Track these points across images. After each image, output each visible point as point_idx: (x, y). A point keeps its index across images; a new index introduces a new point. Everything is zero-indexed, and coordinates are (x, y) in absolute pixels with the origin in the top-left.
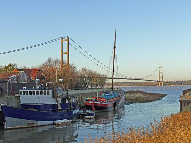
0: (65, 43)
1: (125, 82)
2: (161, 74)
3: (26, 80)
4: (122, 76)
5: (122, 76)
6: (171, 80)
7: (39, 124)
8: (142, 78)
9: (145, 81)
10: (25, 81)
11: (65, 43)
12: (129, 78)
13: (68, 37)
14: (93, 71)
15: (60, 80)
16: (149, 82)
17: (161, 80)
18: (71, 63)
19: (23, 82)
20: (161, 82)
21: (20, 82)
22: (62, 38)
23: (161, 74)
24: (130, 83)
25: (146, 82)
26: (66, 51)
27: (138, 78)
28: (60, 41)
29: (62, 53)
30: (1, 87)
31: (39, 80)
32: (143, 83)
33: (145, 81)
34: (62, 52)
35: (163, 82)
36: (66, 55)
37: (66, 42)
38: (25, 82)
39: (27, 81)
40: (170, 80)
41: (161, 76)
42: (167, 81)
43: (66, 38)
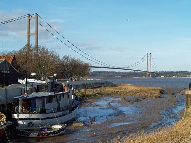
0: (33, 22)
2: (149, 63)
3: (8, 69)
4: (103, 64)
5: (103, 64)
6: (161, 70)
7: (40, 121)
9: (129, 71)
10: (6, 70)
11: (33, 22)
13: (37, 14)
14: (76, 59)
15: (55, 75)
17: (149, 71)
18: (39, 44)
19: (5, 72)
21: (2, 72)
22: (29, 15)
23: (149, 63)
24: (112, 72)
25: (130, 72)
27: (122, 67)
28: (27, 19)
29: (29, 34)
36: (35, 37)
38: (7, 72)
39: (9, 70)
40: (159, 70)
41: (149, 65)
42: (157, 71)
43: (35, 16)
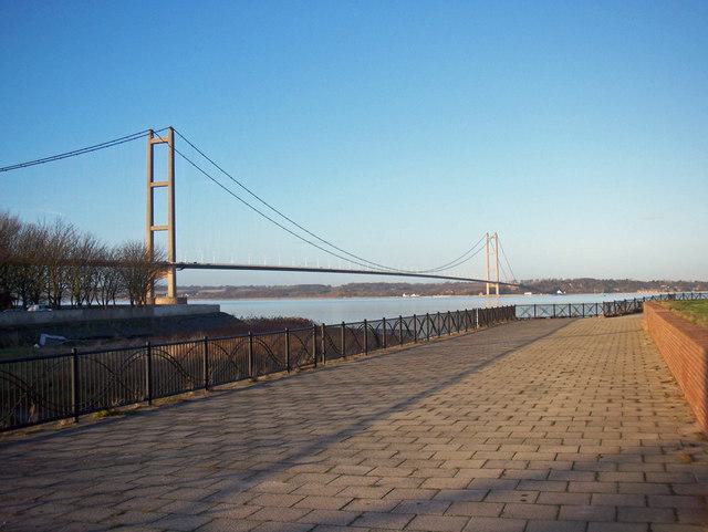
0: (162, 153)
1: (381, 284)
8: (432, 271)
9: (443, 281)
11: (162, 153)
12: (385, 270)
16: (456, 284)
20: (494, 283)
25: (447, 284)
26: (166, 178)
28: (146, 141)
29: (153, 184)
30: (5, 209)
31: (62, 304)
32: (439, 285)
33: (447, 280)
34: (152, 225)
35: (500, 283)
37: (166, 148)
43: (166, 135)
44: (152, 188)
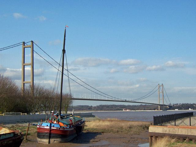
0: (28, 51)
11: (28, 51)
29: (24, 82)
44: (24, 66)
